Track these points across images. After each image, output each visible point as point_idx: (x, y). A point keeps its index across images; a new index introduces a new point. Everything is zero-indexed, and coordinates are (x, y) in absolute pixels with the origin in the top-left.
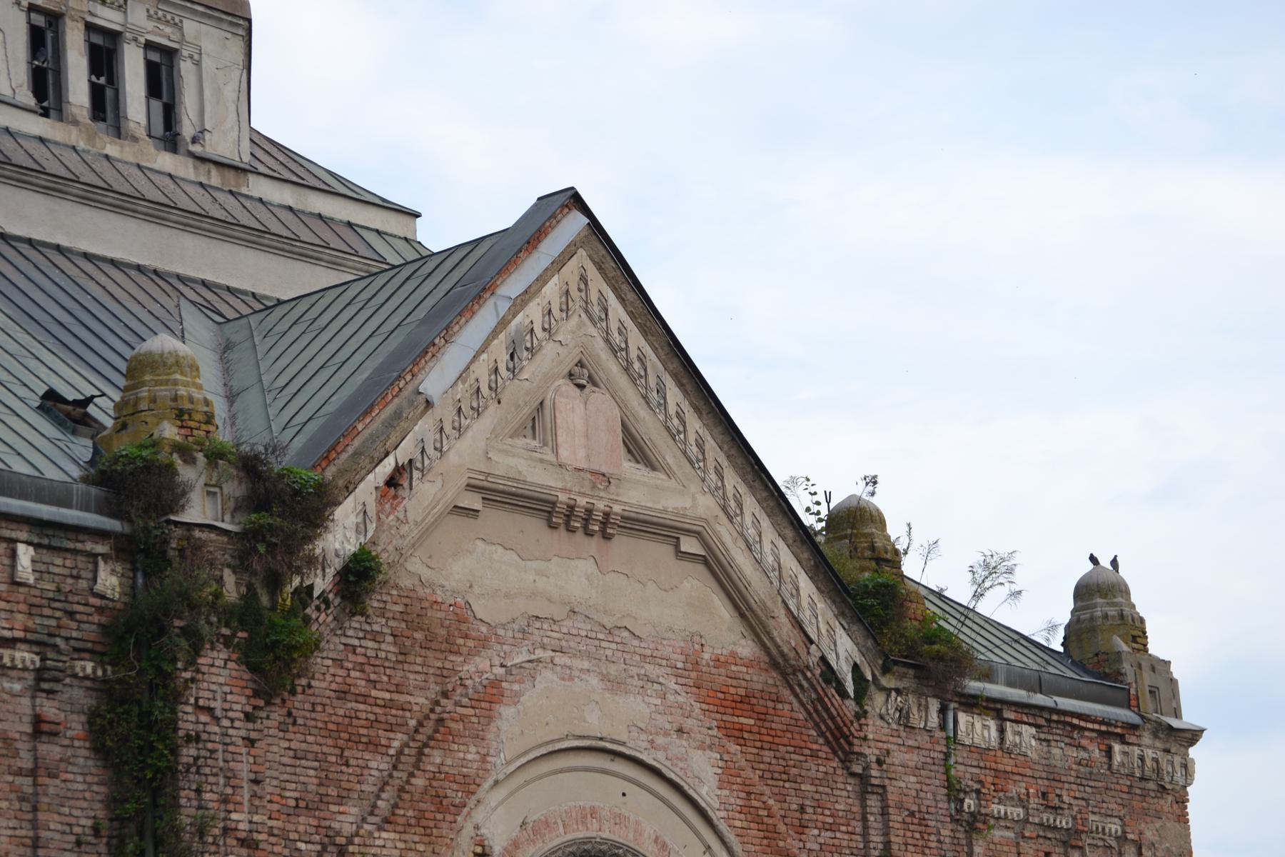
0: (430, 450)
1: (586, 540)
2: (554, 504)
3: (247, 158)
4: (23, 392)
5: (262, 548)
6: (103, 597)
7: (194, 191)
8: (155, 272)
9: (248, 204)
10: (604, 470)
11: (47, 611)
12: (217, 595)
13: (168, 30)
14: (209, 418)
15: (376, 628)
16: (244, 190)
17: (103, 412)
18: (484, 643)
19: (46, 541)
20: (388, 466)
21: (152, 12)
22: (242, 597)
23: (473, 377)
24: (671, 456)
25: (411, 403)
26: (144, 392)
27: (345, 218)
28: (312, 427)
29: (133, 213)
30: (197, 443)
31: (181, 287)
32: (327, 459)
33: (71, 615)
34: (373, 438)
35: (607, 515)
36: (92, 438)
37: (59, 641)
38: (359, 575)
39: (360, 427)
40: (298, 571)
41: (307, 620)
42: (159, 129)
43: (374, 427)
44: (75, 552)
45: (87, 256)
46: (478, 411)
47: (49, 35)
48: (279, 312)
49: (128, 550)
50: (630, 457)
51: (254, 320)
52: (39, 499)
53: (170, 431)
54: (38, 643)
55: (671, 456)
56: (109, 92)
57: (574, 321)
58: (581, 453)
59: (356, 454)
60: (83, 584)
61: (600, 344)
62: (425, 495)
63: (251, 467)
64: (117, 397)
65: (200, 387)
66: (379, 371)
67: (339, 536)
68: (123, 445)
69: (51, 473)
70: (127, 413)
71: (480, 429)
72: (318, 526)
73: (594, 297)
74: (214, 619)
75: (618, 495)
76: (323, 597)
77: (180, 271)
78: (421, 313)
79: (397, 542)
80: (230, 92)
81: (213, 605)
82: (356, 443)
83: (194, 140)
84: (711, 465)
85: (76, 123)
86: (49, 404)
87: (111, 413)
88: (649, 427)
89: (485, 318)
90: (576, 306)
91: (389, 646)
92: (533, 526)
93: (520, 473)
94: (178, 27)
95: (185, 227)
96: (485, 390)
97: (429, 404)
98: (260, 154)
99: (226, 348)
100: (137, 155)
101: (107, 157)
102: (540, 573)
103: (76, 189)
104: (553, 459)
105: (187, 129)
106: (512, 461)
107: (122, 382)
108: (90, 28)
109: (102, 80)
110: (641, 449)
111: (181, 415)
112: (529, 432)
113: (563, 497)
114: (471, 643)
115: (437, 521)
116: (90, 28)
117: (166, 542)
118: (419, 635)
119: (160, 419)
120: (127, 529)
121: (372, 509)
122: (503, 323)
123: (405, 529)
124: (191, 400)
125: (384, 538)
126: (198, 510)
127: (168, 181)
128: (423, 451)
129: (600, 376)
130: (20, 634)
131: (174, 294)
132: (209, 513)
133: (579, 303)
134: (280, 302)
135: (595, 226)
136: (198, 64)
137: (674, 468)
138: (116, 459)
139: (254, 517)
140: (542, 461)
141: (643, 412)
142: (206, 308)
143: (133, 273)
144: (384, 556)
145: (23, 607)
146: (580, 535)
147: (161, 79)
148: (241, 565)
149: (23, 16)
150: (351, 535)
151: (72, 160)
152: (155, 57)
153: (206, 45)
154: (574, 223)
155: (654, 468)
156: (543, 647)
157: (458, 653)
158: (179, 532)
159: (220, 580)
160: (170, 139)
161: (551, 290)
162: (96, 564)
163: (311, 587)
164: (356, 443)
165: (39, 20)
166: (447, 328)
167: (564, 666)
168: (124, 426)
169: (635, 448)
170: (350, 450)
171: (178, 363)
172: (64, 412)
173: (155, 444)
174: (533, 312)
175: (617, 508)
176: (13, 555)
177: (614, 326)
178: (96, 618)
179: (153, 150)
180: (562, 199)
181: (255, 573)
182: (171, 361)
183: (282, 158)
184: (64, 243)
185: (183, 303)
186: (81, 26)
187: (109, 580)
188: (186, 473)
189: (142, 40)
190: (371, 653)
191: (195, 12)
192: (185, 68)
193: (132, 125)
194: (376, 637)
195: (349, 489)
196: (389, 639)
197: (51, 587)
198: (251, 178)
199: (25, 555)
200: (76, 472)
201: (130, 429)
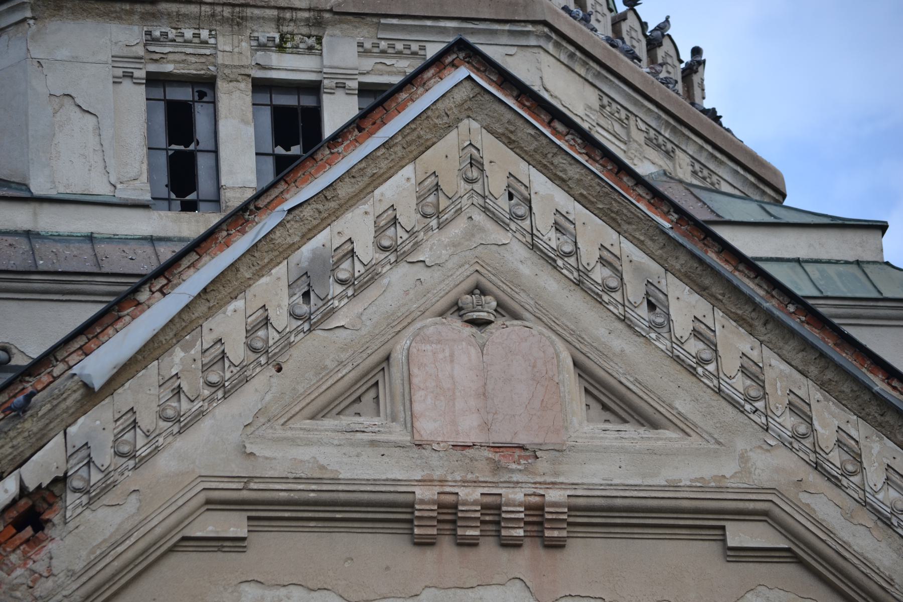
1: (505, 555)
10: (522, 439)
21: (368, 45)
24: (685, 398)
50: (607, 415)
55: (685, 398)
75: (556, 474)
84: (778, 397)
88: (631, 359)
93: (322, 468)
104: (398, 434)
108: (261, 86)
110: (622, 398)
113: (421, 493)
129: (521, 300)
137: (696, 418)
141: (620, 342)
155: (654, 426)
169: (611, 400)
186: (246, 86)
189: (354, 85)
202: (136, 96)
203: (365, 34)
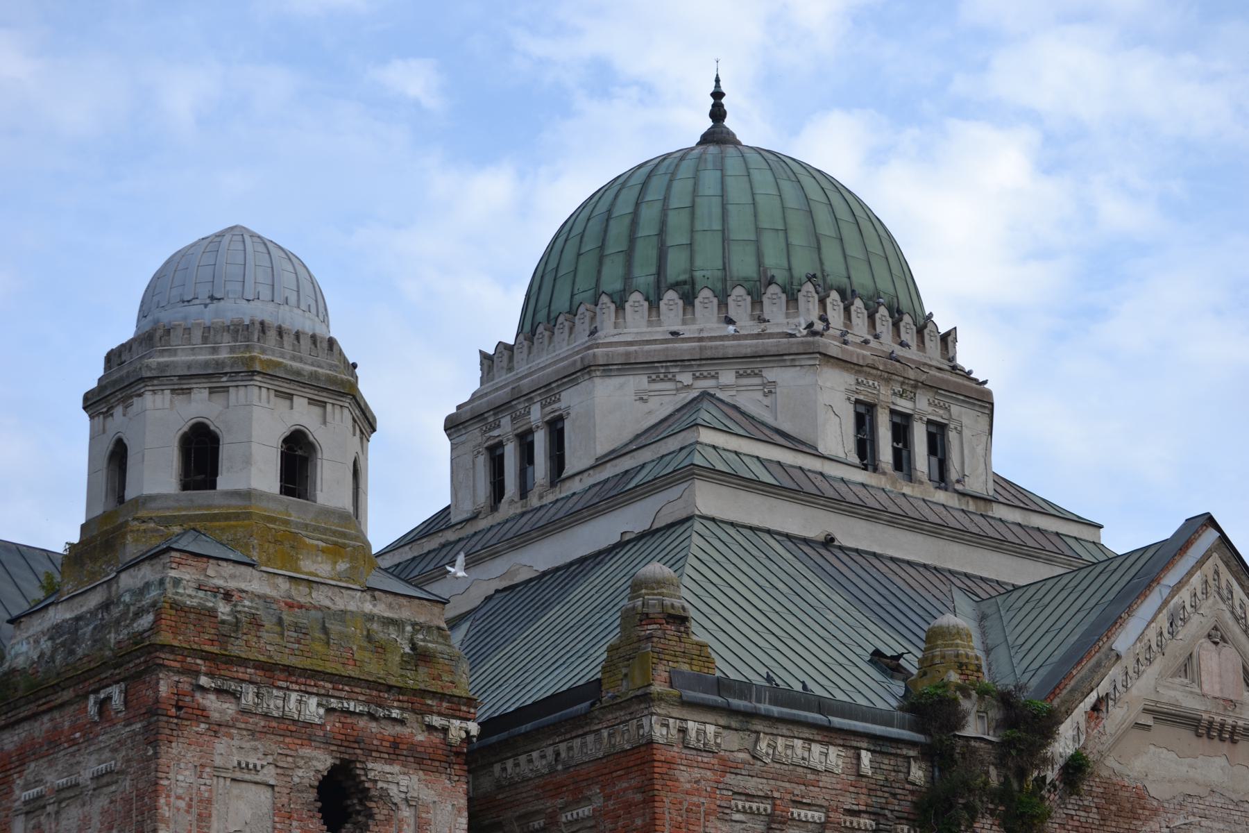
0: (1119, 687)
1: (1221, 744)
2: (1199, 720)
3: (991, 493)
4: (859, 651)
5: (1014, 752)
6: (914, 784)
7: (958, 515)
8: (935, 568)
9: (992, 522)
11: (879, 793)
12: (986, 783)
13: (941, 412)
14: (979, 669)
15: (1086, 803)
16: (990, 514)
17: (911, 664)
18: (1155, 812)
19: (878, 749)
20: (1092, 698)
22: (1002, 784)
23: (1146, 638)
25: (1107, 656)
26: (937, 652)
27: (1054, 530)
28: (1043, 672)
29: (921, 531)
30: (971, 684)
31: (952, 578)
32: (1054, 693)
33: (894, 795)
34: (1083, 680)
35: (1234, 727)
36: (904, 680)
37: (887, 812)
38: (1076, 768)
39: (1074, 672)
40: (1037, 767)
41: (1042, 798)
42: (936, 476)
43: (1083, 672)
44: (896, 755)
45: (892, 559)
46: (1150, 661)
47: (867, 418)
48: (1016, 594)
49: (929, 754)
51: (1000, 599)
52: (874, 722)
53: (954, 677)
54: (874, 814)
56: (904, 453)
57: (1211, 600)
58: (1217, 687)
59: (1073, 690)
60: (901, 776)
61: (1228, 615)
62: (1117, 716)
63: (1006, 699)
64: (920, 655)
65: (973, 648)
66: (1087, 634)
67: (1062, 744)
68: (924, 686)
69: (880, 705)
70: (927, 665)
71: (1151, 673)
72: (1049, 738)
73: (1224, 584)
74: (985, 799)
76: (1052, 783)
77: (951, 567)
78: (1111, 596)
79: (1100, 747)
80: (980, 450)
81: (983, 789)
82: (1072, 683)
83: (958, 481)
85: (884, 473)
86: (876, 658)
87: (916, 664)
89: (1154, 599)
90: (1212, 590)
91: (1094, 815)
92: (1186, 735)
94: (948, 409)
95: (954, 539)
96: (1154, 647)
97: (1118, 657)
98: (999, 489)
99: (983, 618)
100: (922, 493)
101: (904, 495)
102: (1191, 766)
103: (885, 516)
104: (1197, 690)
105: (953, 475)
106: (1172, 693)
107: (923, 646)
108: (893, 412)
109: (900, 446)
111: (961, 667)
112: (1183, 673)
113: (1205, 716)
114: (1147, 813)
115: (1125, 732)
116: (893, 412)
117: (953, 749)
118: (1113, 808)
119: (948, 669)
120: (929, 740)
121: (1083, 726)
122: (1165, 603)
123: (1104, 738)
124: (967, 656)
125: (1090, 744)
126: (973, 728)
127: (942, 509)
128: (1115, 688)
129: (1228, 636)
130: (863, 808)
131: (947, 583)
132: (980, 729)
133: (1214, 588)
134: (1016, 588)
135: (1224, 538)
136: (960, 433)
138: (921, 695)
139: (1008, 732)
140: (1191, 692)
142: (968, 592)
143: (921, 569)
144: (1091, 756)
145: (865, 791)
146: (1216, 740)
147: (937, 443)
148: (1001, 764)
149: (851, 407)
150: (1070, 743)
151: (882, 497)
152: (933, 429)
153: (965, 421)
154: (1210, 536)
156: (1194, 815)
157: (1138, 819)
158: (961, 742)
159: (987, 773)
160: (942, 478)
161: (1196, 580)
162: (909, 763)
163: (1045, 777)
164: (1072, 683)
165: (862, 409)
166: (1130, 606)
167: (1208, 827)
168: (925, 674)
170: (1069, 688)
171: (959, 633)
172: (886, 664)
173: (945, 686)
174: (1185, 595)
175: (1240, 723)
176: (859, 757)
177: (1237, 603)
178: (909, 798)
179: (932, 489)
180: (1201, 521)
181: (1009, 769)
182: (954, 631)
183: (1013, 491)
184: (878, 551)
185: (954, 588)
186: (887, 411)
187: (917, 773)
188: (965, 704)
190: (1083, 820)
191: (958, 400)
192: (952, 435)
193: (919, 474)
194: (1086, 809)
195: (1068, 712)
196: (1095, 810)
197: (882, 778)
198: (995, 505)
199: (866, 757)
200: (895, 703)
201: (929, 676)
202: (851, 408)
203: (930, 395)
